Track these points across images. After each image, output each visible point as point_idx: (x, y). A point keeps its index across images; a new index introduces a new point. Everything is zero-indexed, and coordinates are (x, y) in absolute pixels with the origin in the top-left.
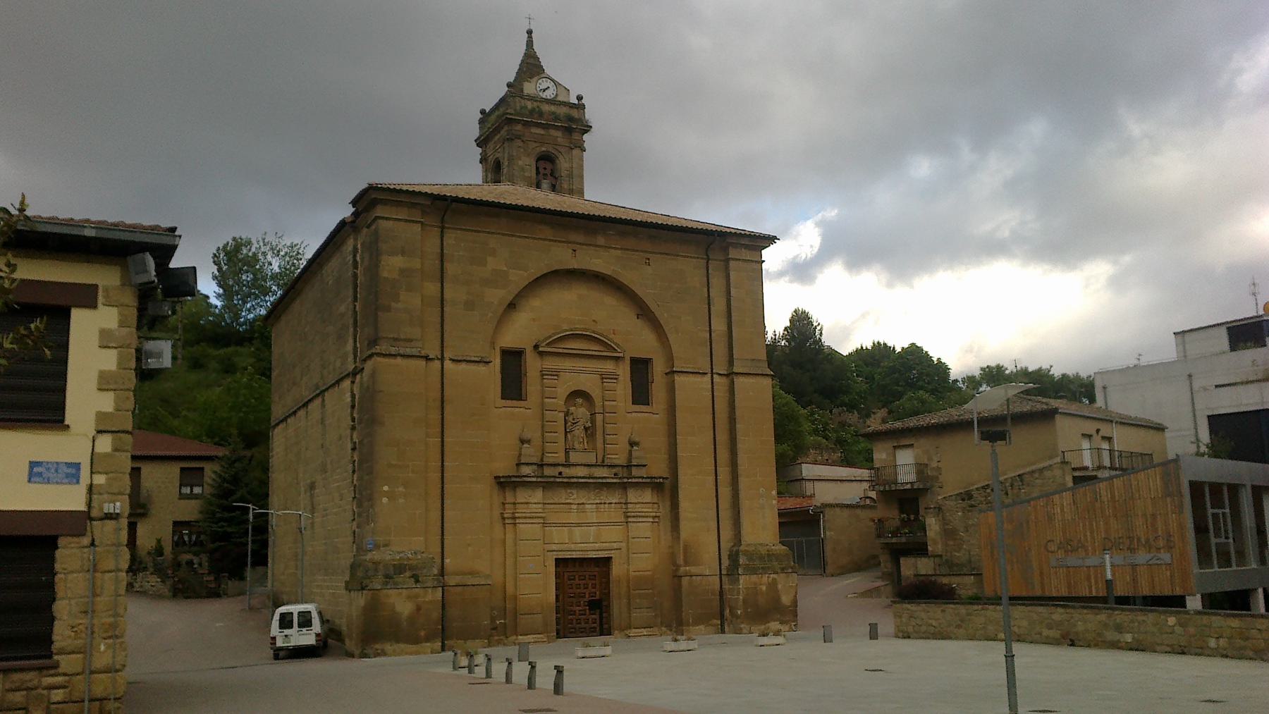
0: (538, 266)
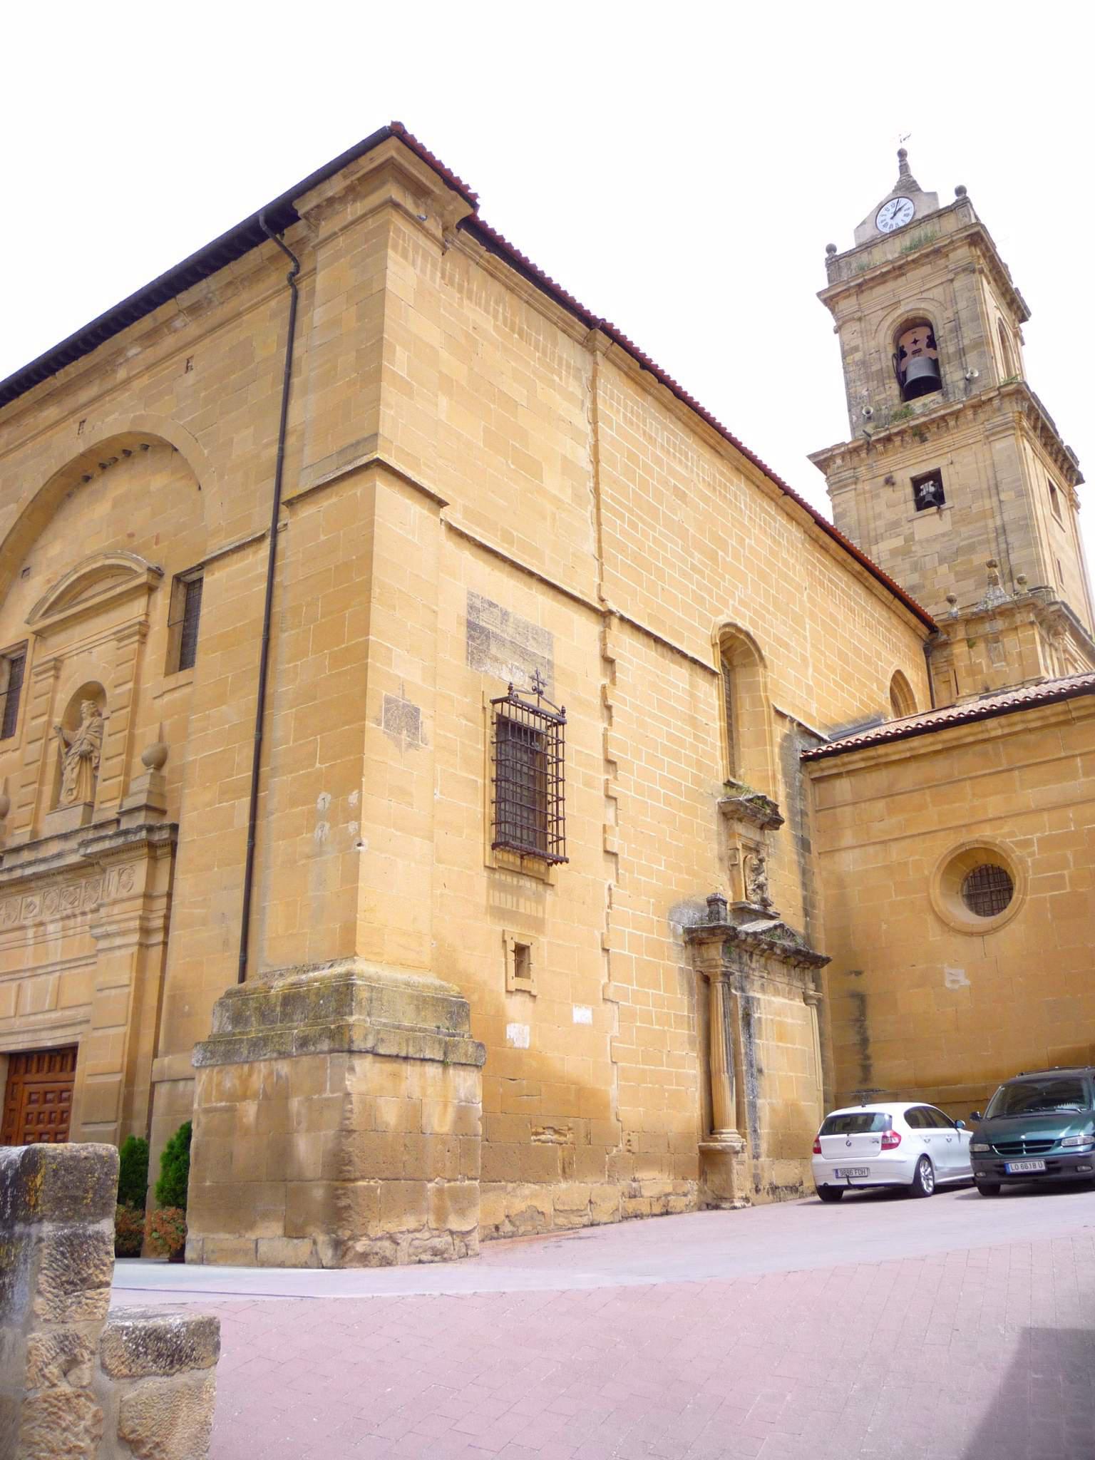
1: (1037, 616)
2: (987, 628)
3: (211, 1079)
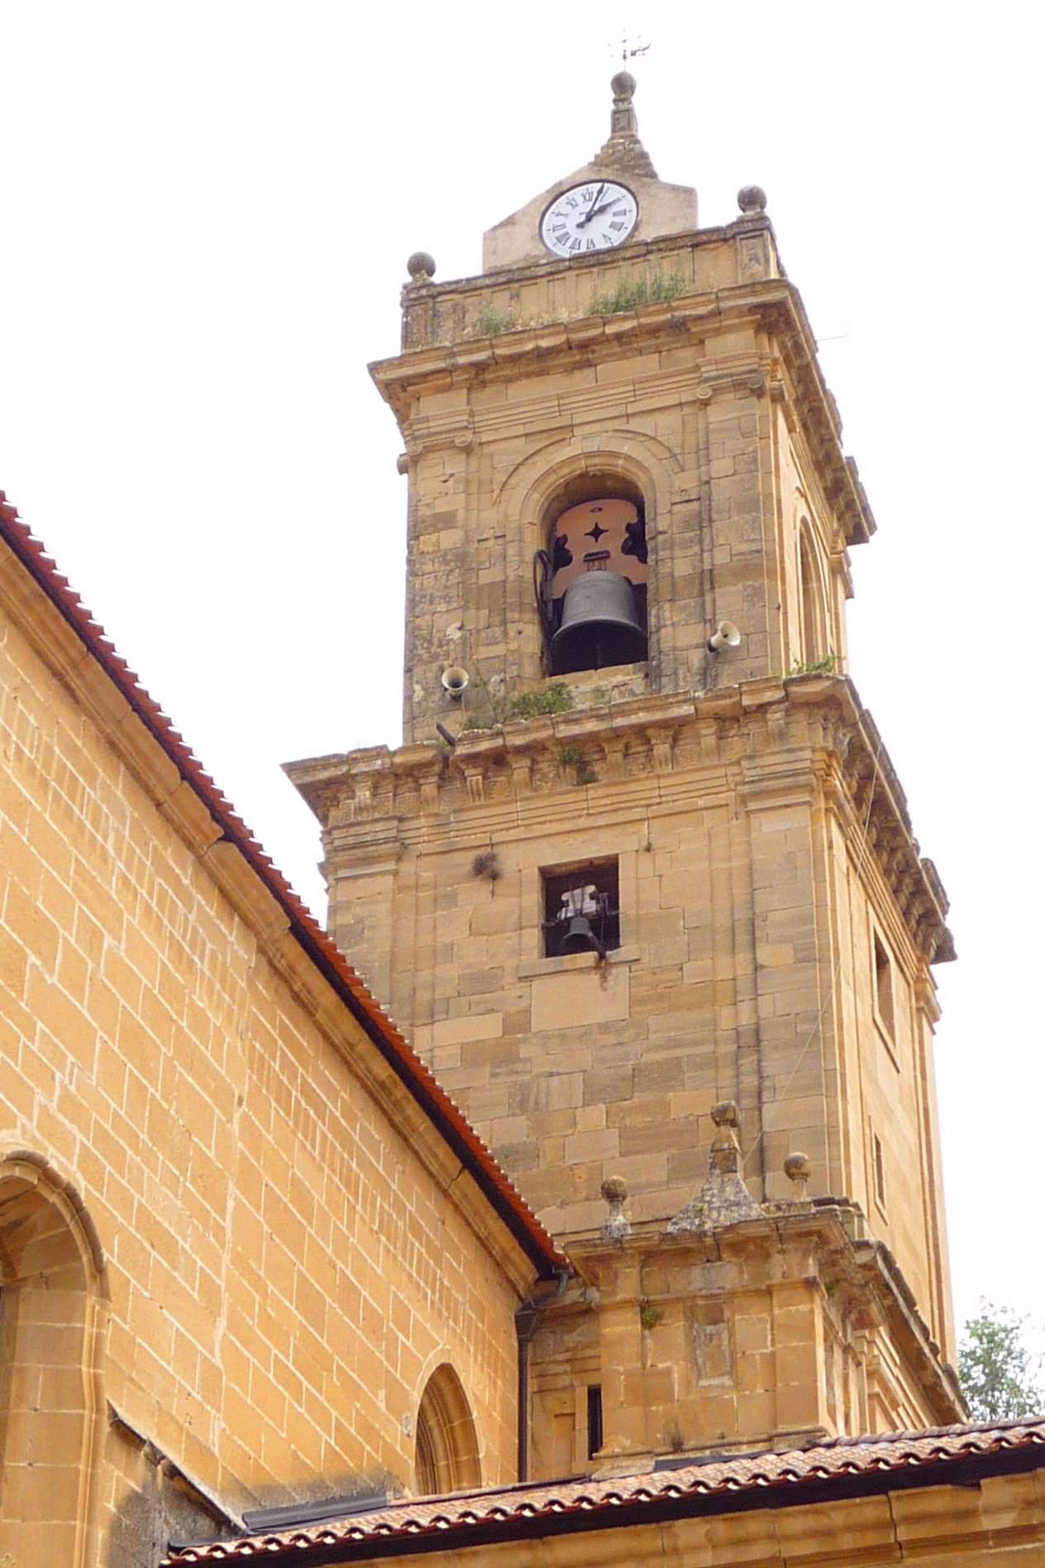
1: (822, 1267)
2: (696, 1279)
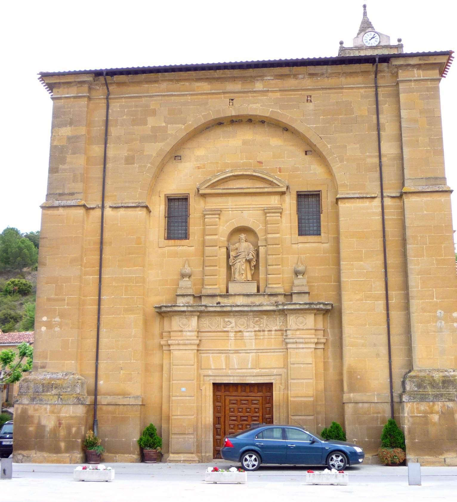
0: (197, 117)
3: (413, 407)
